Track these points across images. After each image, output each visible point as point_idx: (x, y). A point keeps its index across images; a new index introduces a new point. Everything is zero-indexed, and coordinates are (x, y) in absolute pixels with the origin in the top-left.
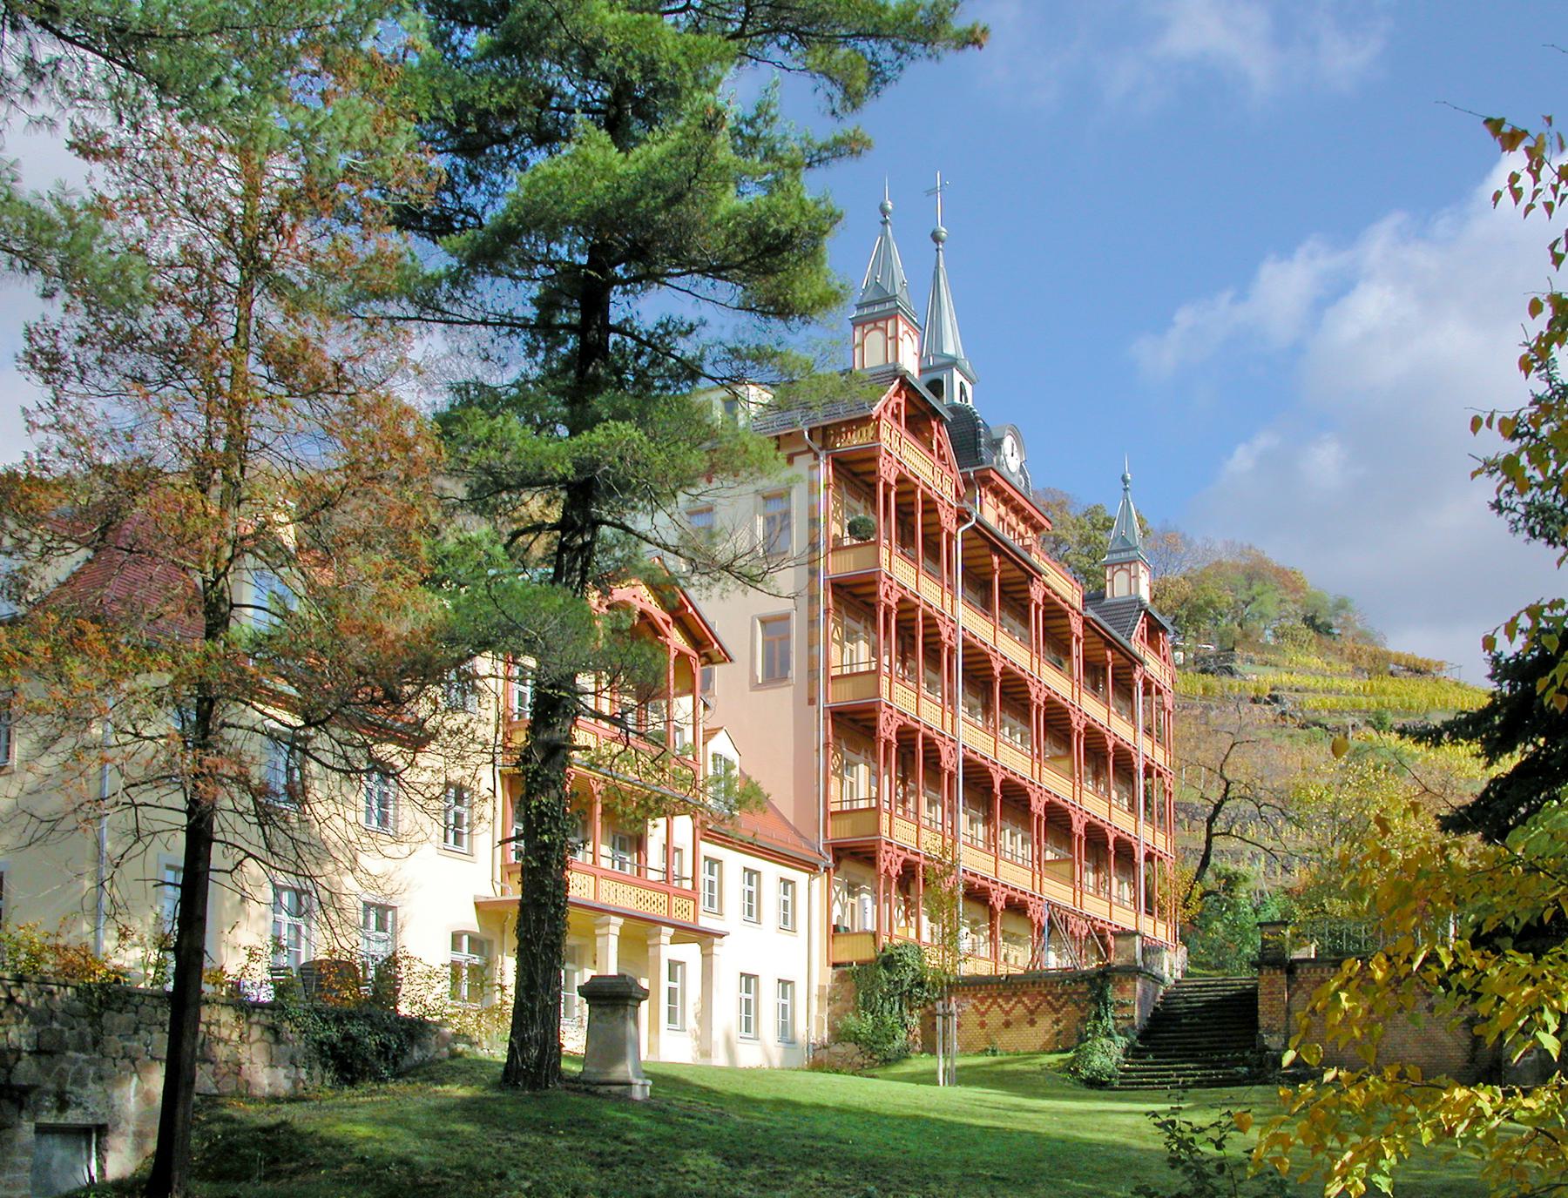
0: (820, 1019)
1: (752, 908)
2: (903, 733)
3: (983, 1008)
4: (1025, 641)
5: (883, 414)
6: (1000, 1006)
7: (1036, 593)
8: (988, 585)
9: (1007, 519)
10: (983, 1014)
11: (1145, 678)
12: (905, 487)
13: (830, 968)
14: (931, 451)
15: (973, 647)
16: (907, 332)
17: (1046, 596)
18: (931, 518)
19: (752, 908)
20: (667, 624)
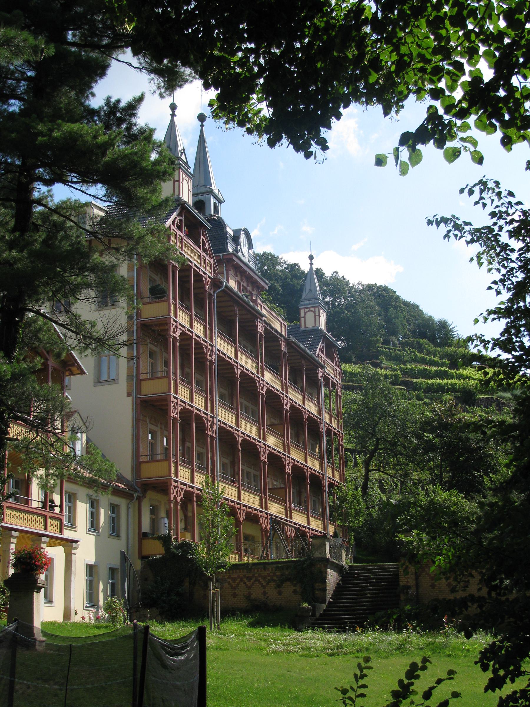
3: (234, 585)
6: (245, 583)
9: (242, 283)
10: (234, 588)
11: (325, 376)
17: (266, 329)
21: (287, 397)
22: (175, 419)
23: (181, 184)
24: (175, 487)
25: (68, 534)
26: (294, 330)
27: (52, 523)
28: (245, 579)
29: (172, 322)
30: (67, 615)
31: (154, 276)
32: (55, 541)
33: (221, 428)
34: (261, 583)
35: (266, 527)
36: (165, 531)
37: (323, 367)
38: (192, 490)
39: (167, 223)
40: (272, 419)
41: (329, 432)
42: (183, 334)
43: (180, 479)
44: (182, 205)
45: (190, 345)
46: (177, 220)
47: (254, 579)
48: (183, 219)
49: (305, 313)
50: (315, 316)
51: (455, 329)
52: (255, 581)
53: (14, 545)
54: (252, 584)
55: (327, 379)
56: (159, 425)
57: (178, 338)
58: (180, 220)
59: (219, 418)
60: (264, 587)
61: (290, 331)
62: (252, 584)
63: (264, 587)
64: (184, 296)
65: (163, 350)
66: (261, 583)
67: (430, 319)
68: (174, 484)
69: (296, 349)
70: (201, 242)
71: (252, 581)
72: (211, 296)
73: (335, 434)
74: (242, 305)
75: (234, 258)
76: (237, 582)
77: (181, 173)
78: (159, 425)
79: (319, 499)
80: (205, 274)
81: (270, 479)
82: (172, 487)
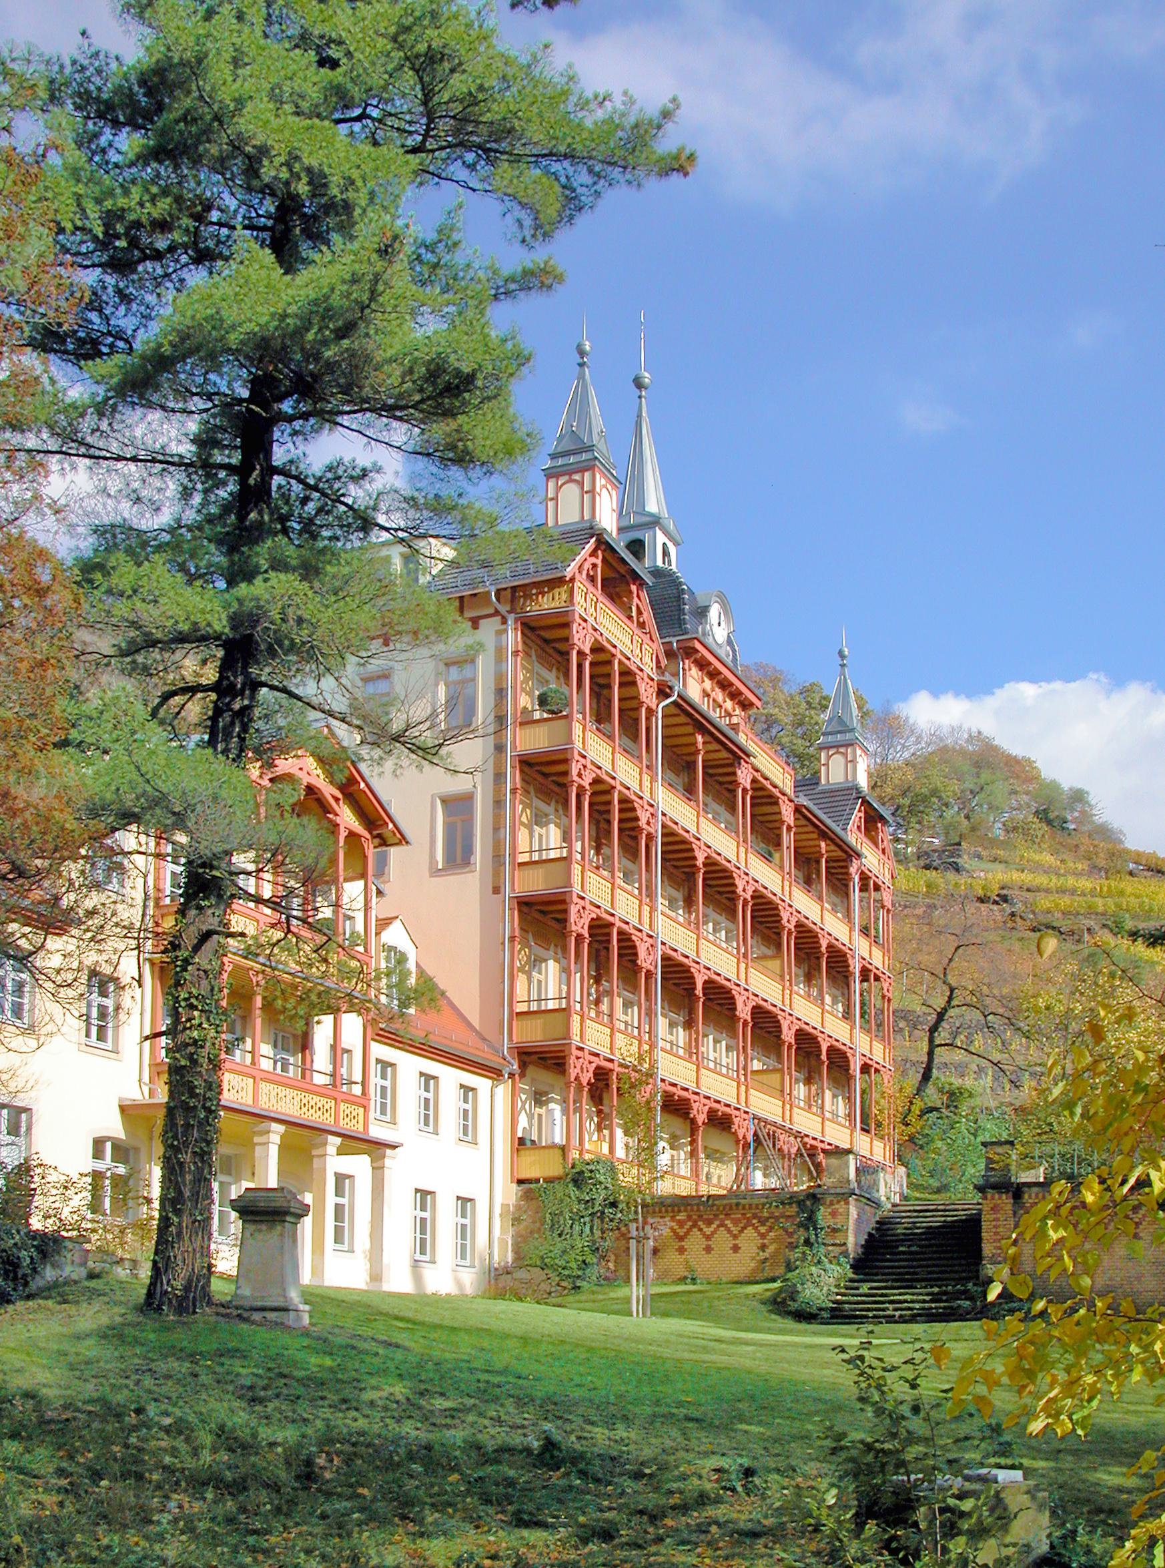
0: (502, 1241)
1: (429, 1116)
2: (600, 927)
4: (731, 829)
5: (577, 575)
6: (700, 1230)
7: (744, 776)
8: (690, 766)
10: (708, 1238)
11: (862, 872)
12: (602, 657)
13: (515, 1185)
14: (630, 618)
15: (673, 834)
16: (605, 486)
17: (754, 781)
18: (629, 692)
19: (429, 1116)
20: (337, 800)
21: (791, 906)
22: (579, 937)
23: (597, 497)
24: (578, 1058)
25: (377, 1132)
26: (807, 783)
27: (347, 1112)
28: (700, 1223)
29: (577, 757)
30: (376, 1276)
31: (545, 673)
32: (356, 1143)
33: (666, 958)
34: (729, 1231)
35: (744, 1137)
36: (559, 1139)
37: (859, 856)
38: (611, 919)
39: (568, 569)
40: (763, 948)
41: (865, 973)
42: (597, 781)
43: (591, 1045)
44: (603, 545)
45: (609, 935)
46: (587, 566)
47: (717, 1223)
48: (599, 562)
49: (829, 757)
50: (847, 762)
51: (1100, 806)
52: (718, 1226)
53: (278, 1137)
54: (713, 1233)
55: (864, 878)
56: (553, 803)
57: (588, 787)
58: (594, 566)
59: (661, 1073)
60: (735, 1237)
61: (799, 785)
62: (713, 1233)
63: (735, 1237)
64: (601, 716)
65: (561, 812)
66: (729, 1231)
67: (1054, 786)
68: (575, 1052)
69: (808, 819)
70: (634, 609)
71: (714, 1226)
72: (650, 712)
73: (877, 979)
74: (712, 734)
75: (698, 646)
76: (687, 1227)
77: (598, 476)
78: (553, 803)
79: (843, 994)
80: (642, 670)
81: (754, 942)
82: (573, 1058)
